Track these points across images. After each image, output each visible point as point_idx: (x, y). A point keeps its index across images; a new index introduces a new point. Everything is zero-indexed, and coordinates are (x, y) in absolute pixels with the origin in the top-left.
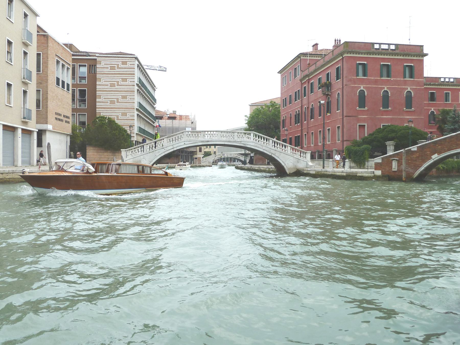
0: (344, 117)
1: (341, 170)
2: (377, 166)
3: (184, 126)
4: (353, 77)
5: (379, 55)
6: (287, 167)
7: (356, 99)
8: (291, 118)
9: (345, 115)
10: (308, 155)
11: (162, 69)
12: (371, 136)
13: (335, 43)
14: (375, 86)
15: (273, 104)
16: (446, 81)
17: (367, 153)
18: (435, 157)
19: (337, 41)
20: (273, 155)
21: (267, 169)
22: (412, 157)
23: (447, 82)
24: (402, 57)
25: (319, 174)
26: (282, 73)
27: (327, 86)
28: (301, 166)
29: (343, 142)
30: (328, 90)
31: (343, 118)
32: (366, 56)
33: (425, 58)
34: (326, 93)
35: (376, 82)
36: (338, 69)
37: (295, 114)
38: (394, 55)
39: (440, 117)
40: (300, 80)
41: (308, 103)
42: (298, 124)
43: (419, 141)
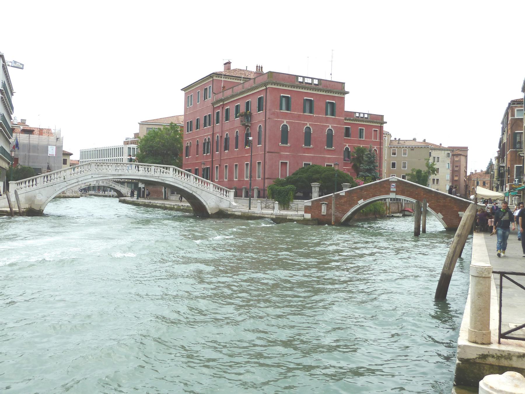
0: (266, 152)
1: (270, 212)
2: (307, 209)
3: (47, 143)
4: (276, 111)
5: (302, 89)
6: (209, 206)
7: (279, 134)
8: (198, 145)
9: (267, 150)
10: (232, 194)
11: (17, 66)
12: (295, 176)
13: (257, 70)
14: (297, 122)
15: (173, 126)
16: (361, 116)
17: (292, 193)
18: (361, 202)
19: (258, 68)
20: (194, 193)
21: (176, 207)
22: (340, 201)
23: (361, 117)
24: (324, 93)
25: (246, 215)
26: (187, 91)
27: (247, 116)
28: (224, 205)
29: (264, 179)
30: (248, 121)
31: (265, 153)
32: (290, 89)
33: (346, 96)
34: (246, 124)
35: (299, 117)
36: (260, 99)
37: (204, 142)
38: (317, 90)
39: (356, 155)
40: (212, 104)
41: (222, 131)
42: (208, 154)
43: (344, 184)
